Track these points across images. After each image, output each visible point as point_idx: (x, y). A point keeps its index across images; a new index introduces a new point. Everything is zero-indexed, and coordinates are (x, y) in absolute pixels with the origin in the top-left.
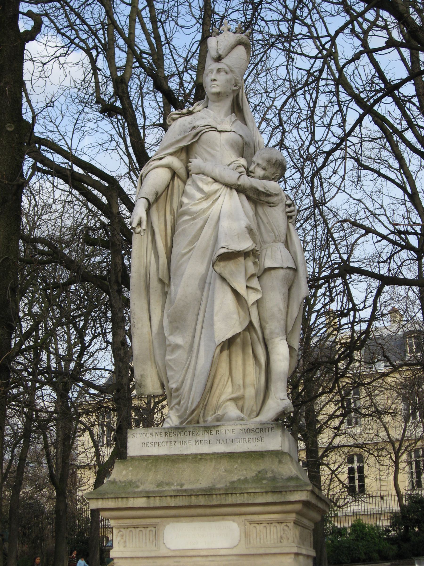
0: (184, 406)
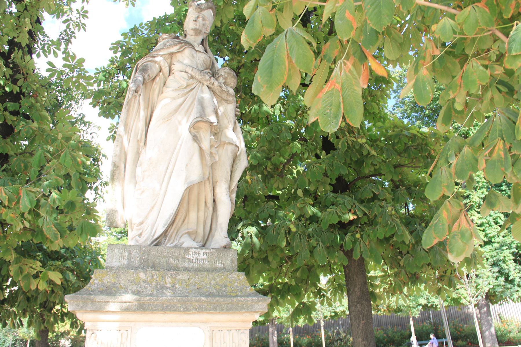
0: (146, 236)
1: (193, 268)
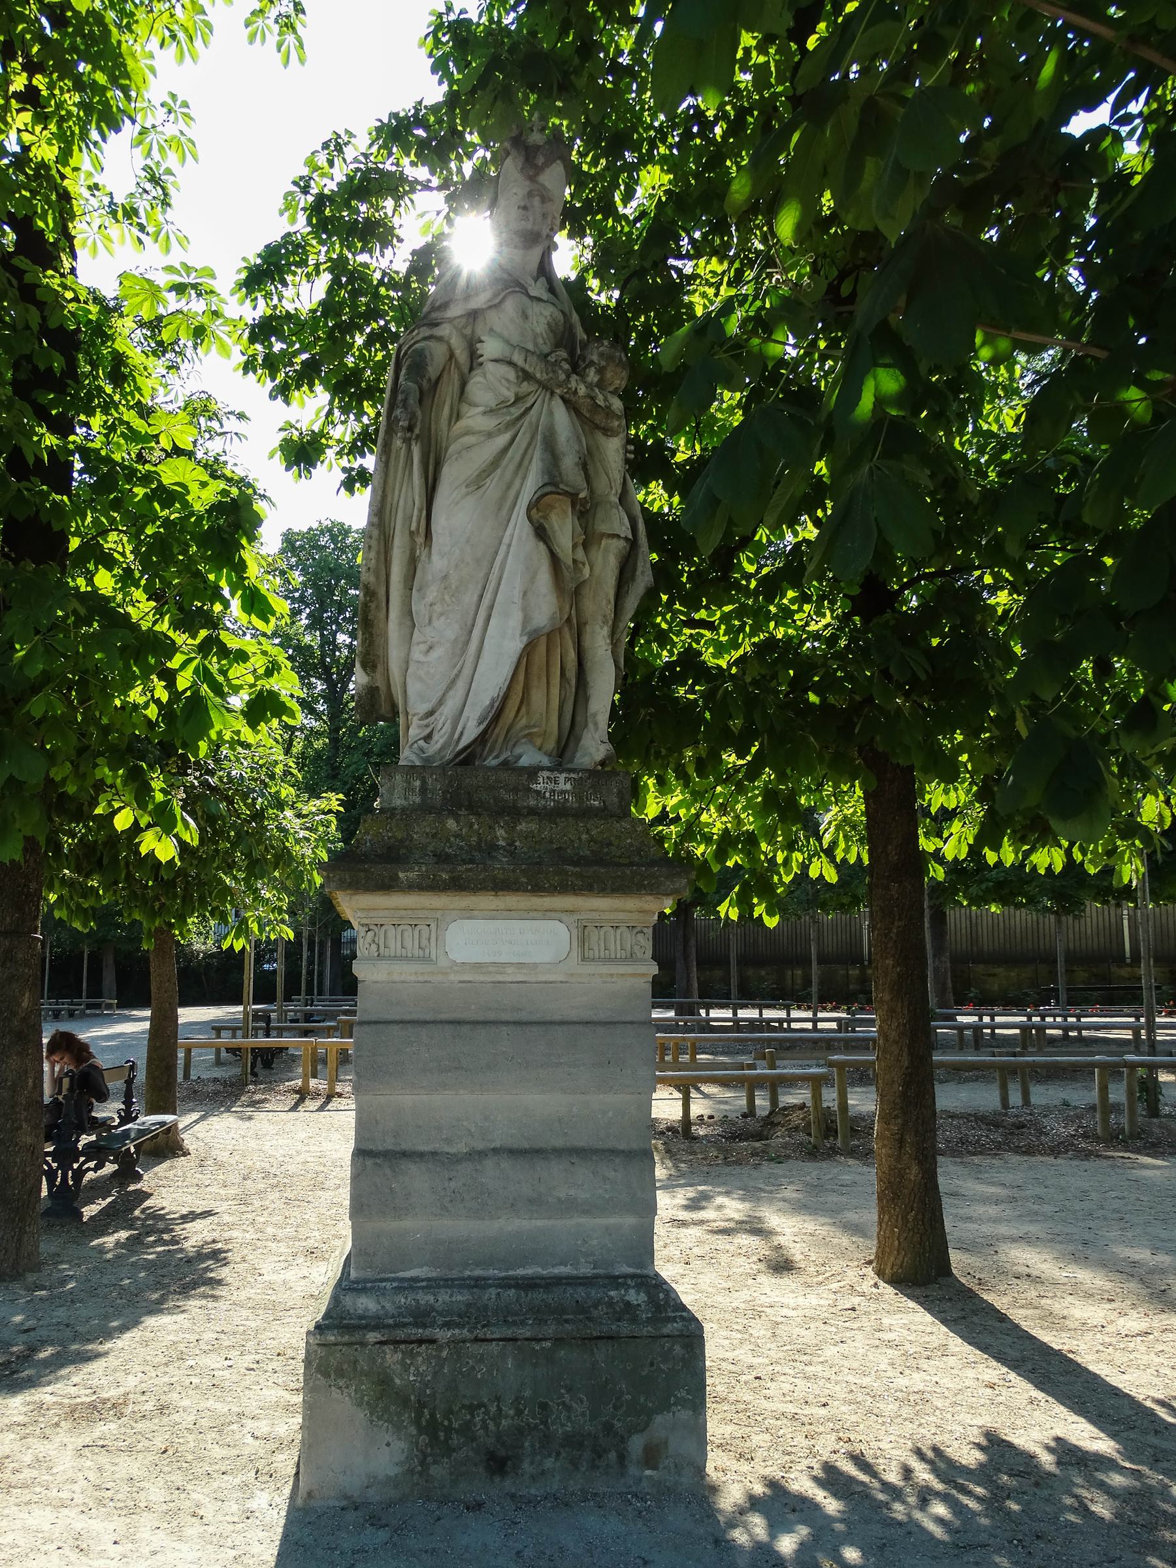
0: (441, 741)
1: (545, 807)
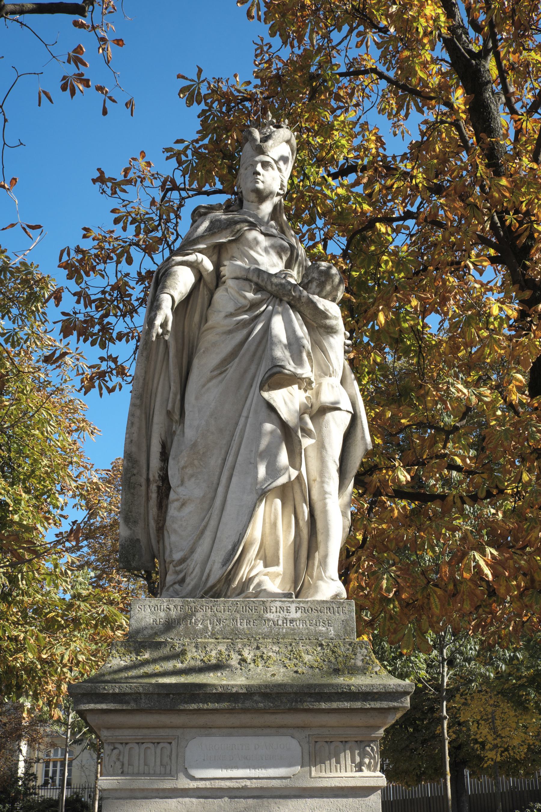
0: (193, 583)
